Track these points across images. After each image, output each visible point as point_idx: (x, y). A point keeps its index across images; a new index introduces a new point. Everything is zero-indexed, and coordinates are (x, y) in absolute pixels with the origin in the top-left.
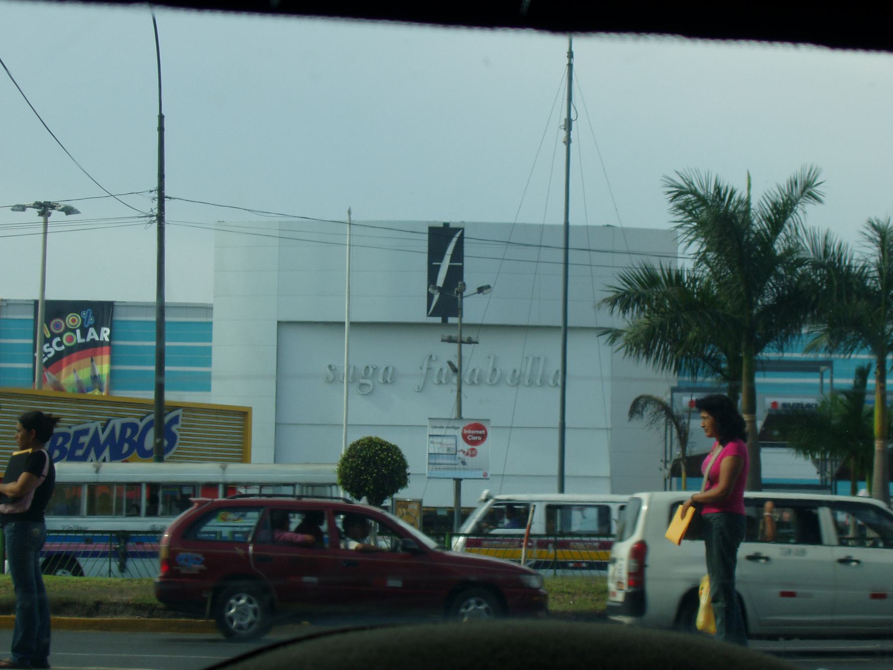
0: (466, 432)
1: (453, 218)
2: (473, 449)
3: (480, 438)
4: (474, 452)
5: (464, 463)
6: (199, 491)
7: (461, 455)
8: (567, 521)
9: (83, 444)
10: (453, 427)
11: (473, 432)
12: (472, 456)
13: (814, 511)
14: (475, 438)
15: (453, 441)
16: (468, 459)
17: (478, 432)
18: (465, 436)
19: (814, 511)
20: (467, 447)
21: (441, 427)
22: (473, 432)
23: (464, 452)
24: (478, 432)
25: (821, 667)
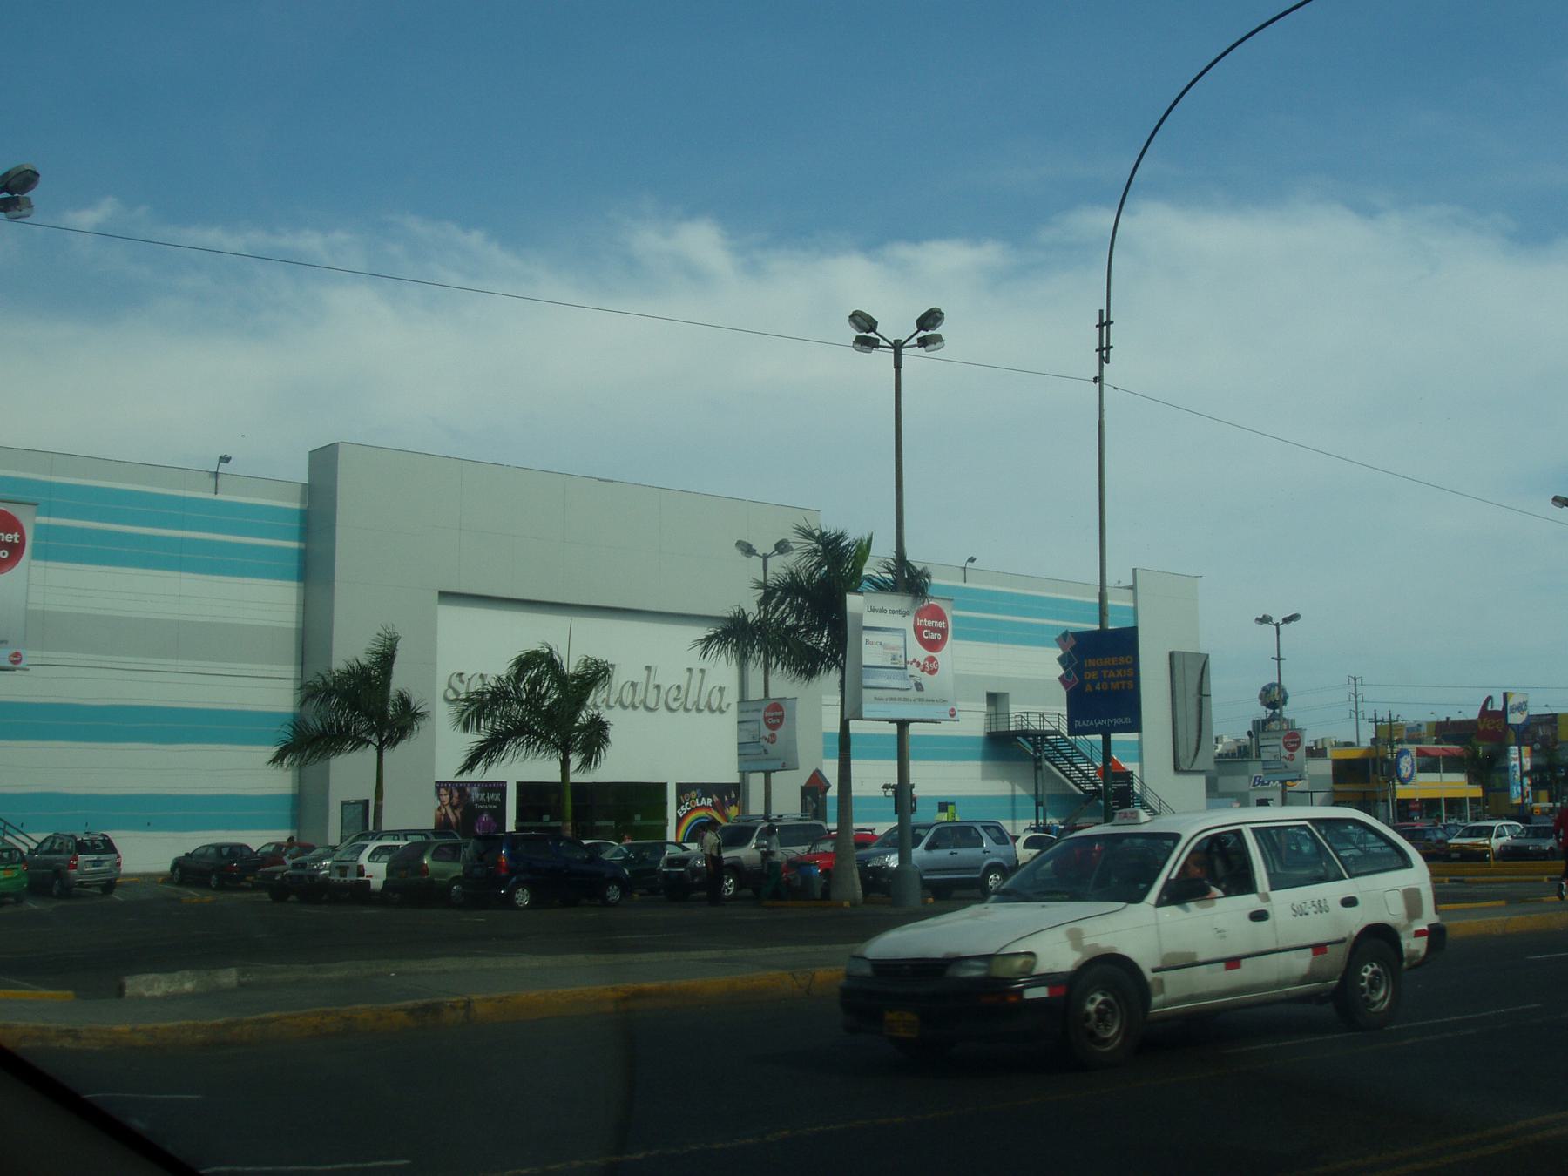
0: (921, 622)
2: (932, 659)
5: (919, 687)
8: (733, 802)
11: (930, 623)
12: (932, 672)
16: (925, 678)
18: (918, 630)
20: (922, 654)
21: (882, 611)
22: (930, 623)
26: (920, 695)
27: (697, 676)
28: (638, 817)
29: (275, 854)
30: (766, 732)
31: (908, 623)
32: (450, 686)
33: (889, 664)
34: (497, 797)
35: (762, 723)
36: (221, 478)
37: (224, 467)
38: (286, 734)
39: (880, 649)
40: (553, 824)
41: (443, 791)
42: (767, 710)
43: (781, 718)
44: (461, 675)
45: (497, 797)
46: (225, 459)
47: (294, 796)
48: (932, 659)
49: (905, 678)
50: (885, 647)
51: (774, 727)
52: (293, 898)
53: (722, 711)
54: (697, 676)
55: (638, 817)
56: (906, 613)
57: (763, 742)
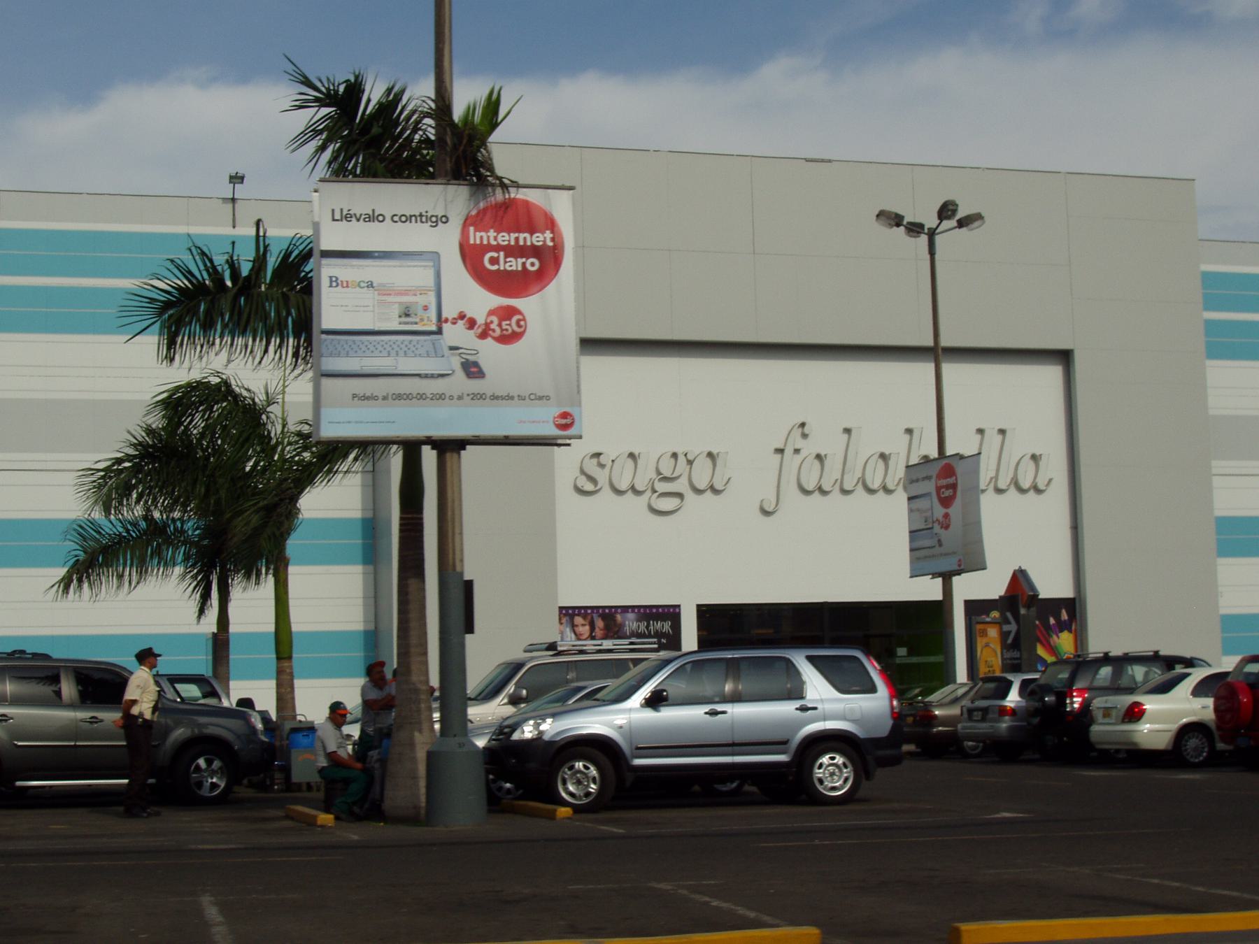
0: (475, 237)
1: (950, 198)
2: (507, 313)
3: (533, 264)
4: (511, 325)
5: (472, 370)
6: (68, 689)
7: (455, 334)
8: (1063, 626)
9: (1198, 691)
10: (420, 218)
11: (505, 238)
12: (508, 338)
13: (1213, 726)
14: (514, 264)
15: (420, 276)
16: (489, 352)
17: (524, 238)
18: (471, 256)
19: (1213, 726)
20: (482, 302)
21: (372, 218)
22: (505, 238)
23: (472, 324)
24: (524, 238)
25: (499, 172)
26: (475, 385)
27: (993, 440)
28: (902, 651)
29: (1096, 673)
30: (939, 511)
31: (446, 241)
32: (583, 472)
33: (395, 326)
34: (667, 627)
35: (935, 500)
36: (238, 205)
37: (240, 191)
38: (71, 548)
39: (368, 296)
40: (914, 660)
41: (578, 620)
42: (939, 477)
43: (954, 486)
44: (598, 455)
45: (667, 627)
46: (237, 179)
47: (366, 633)
48: (507, 313)
49: (436, 353)
50: (385, 291)
51: (946, 502)
52: (1166, 713)
53: (1038, 491)
54: (993, 440)
55: (902, 651)
56: (439, 221)
57: (937, 528)
